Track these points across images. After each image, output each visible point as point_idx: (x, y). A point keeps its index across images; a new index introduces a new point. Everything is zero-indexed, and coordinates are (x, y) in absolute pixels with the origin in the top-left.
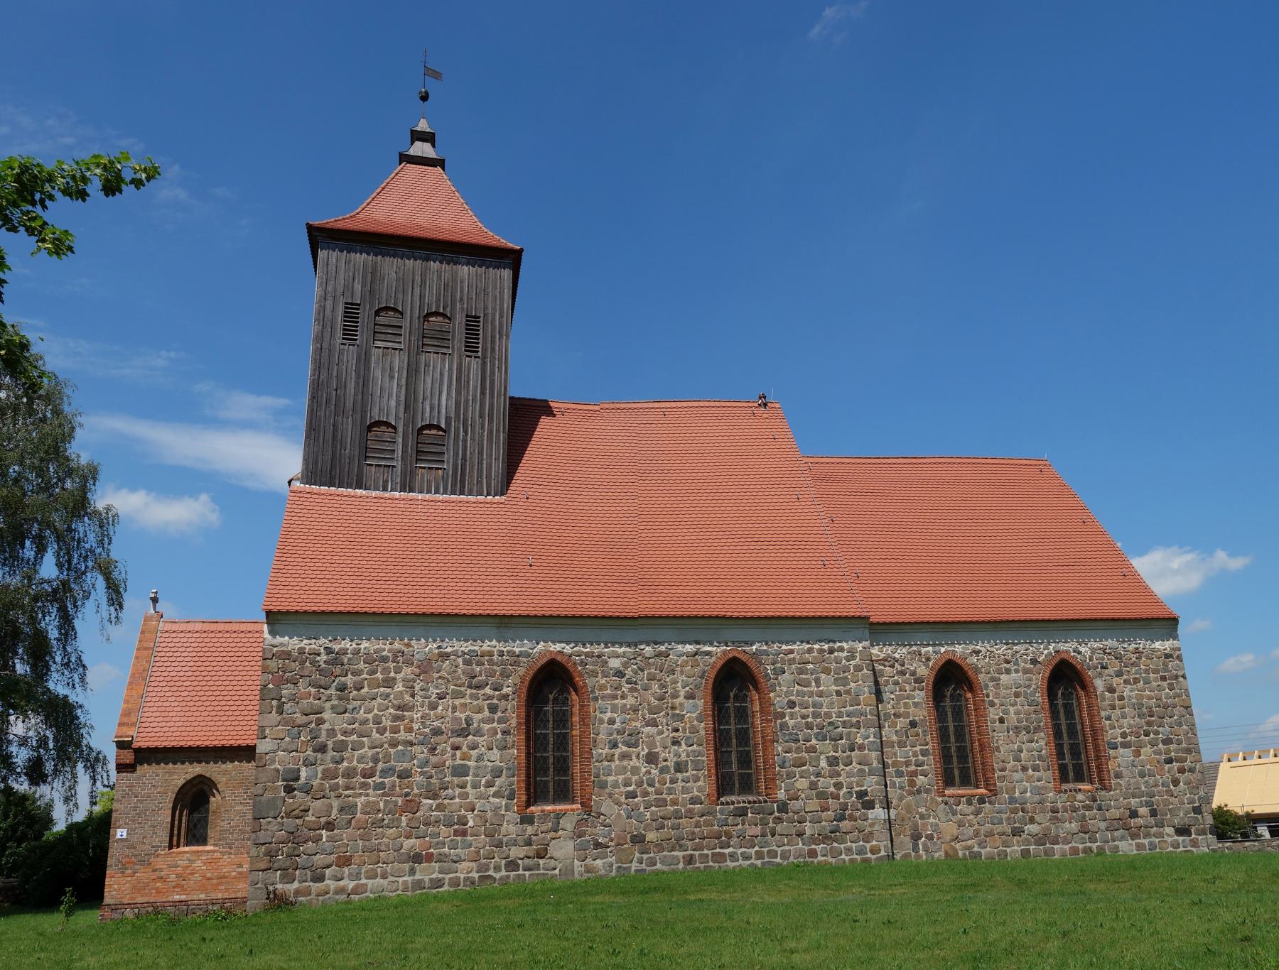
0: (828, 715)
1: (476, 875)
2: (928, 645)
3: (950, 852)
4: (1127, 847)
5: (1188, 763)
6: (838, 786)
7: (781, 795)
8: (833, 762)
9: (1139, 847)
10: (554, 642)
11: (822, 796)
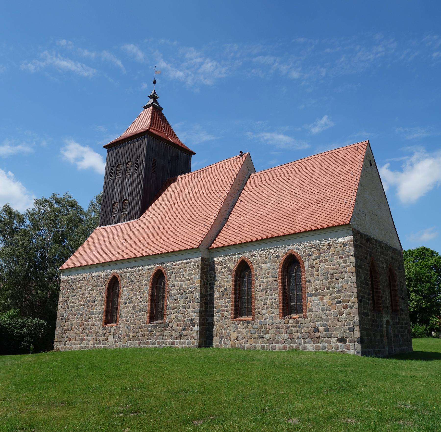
0: (184, 289)
1: (92, 345)
2: (235, 255)
3: (233, 345)
4: (310, 347)
5: (350, 303)
6: (184, 317)
7: (167, 321)
8: (184, 307)
9: (317, 347)
10: (115, 270)
11: (179, 321)
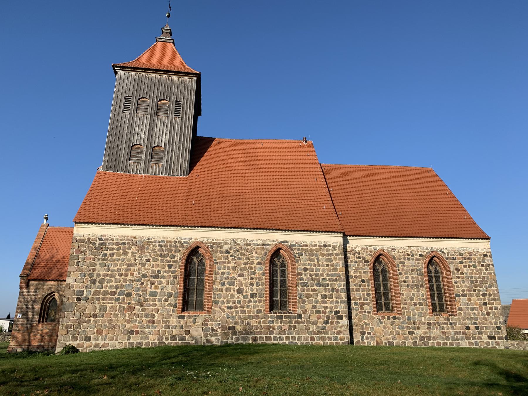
5: (494, 305)
6: (326, 308)
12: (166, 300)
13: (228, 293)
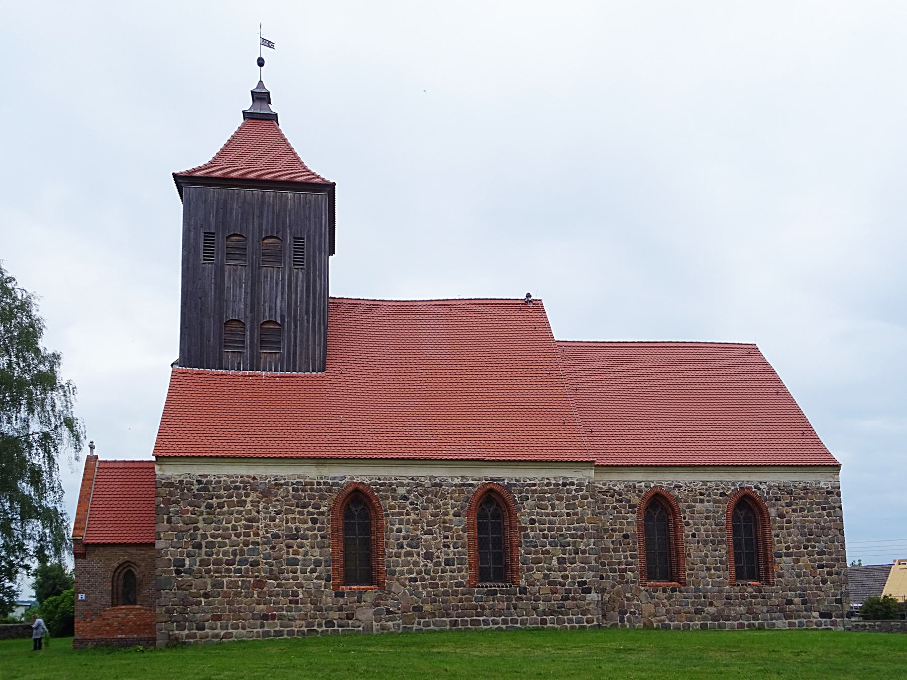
5: (836, 568)
6: (565, 577)
7: (523, 582)
8: (561, 561)
12: (313, 571)
13: (409, 558)
